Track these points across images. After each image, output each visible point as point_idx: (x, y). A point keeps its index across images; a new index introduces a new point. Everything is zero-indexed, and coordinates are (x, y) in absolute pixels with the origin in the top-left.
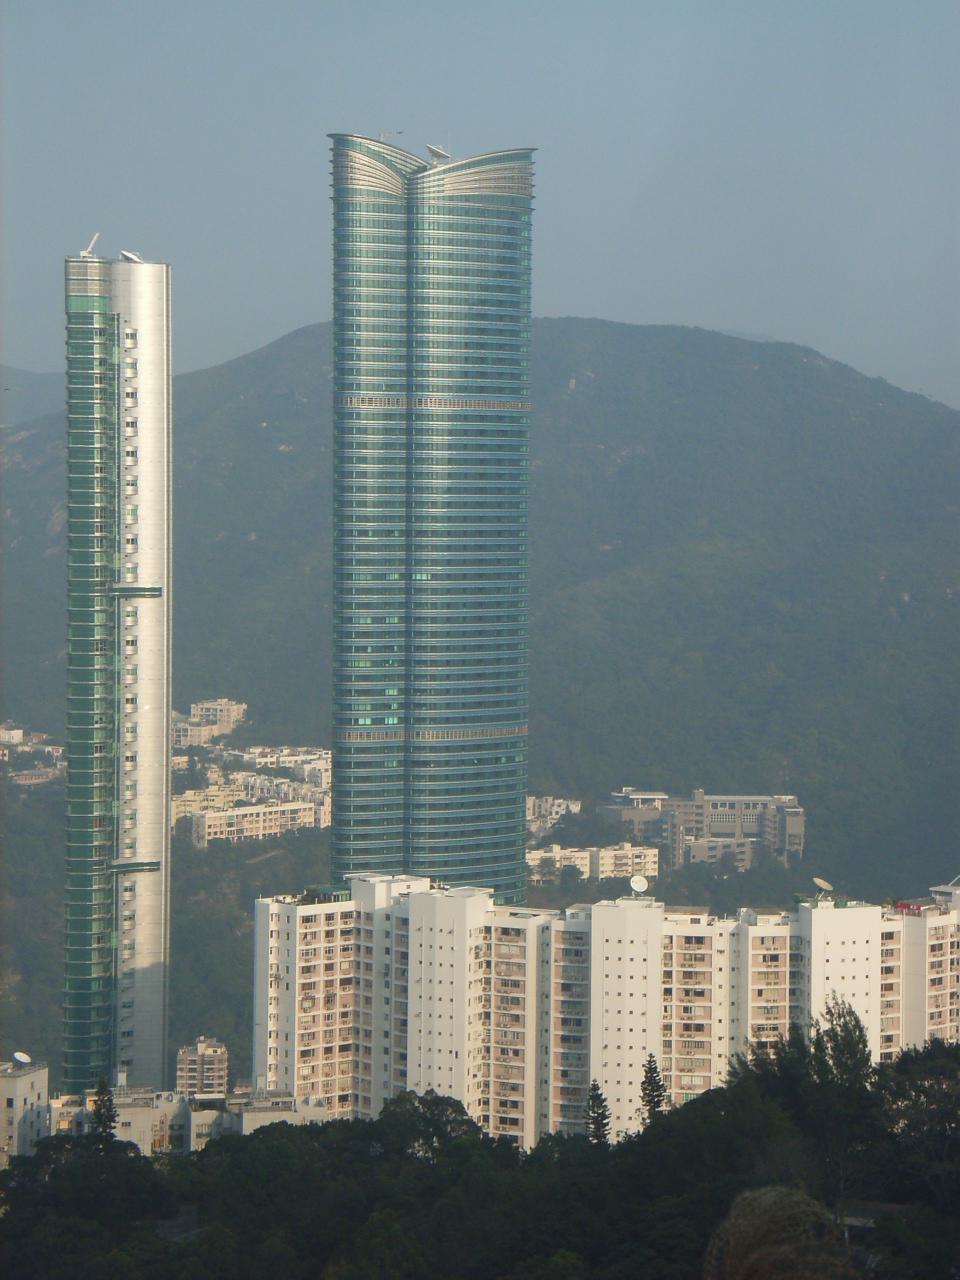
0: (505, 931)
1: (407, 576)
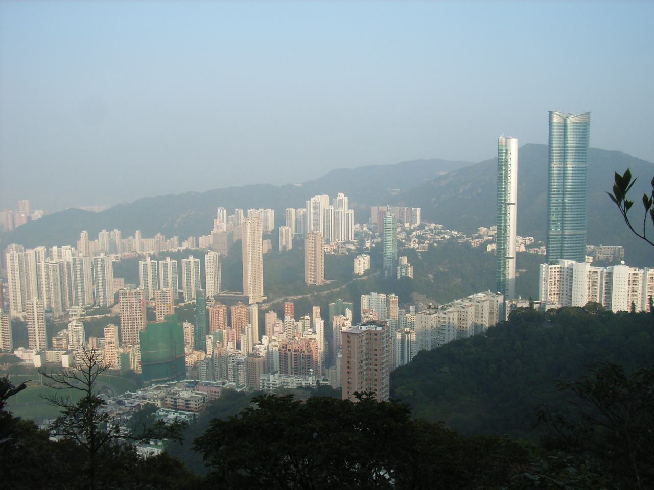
0: (594, 272)
1: (563, 200)
